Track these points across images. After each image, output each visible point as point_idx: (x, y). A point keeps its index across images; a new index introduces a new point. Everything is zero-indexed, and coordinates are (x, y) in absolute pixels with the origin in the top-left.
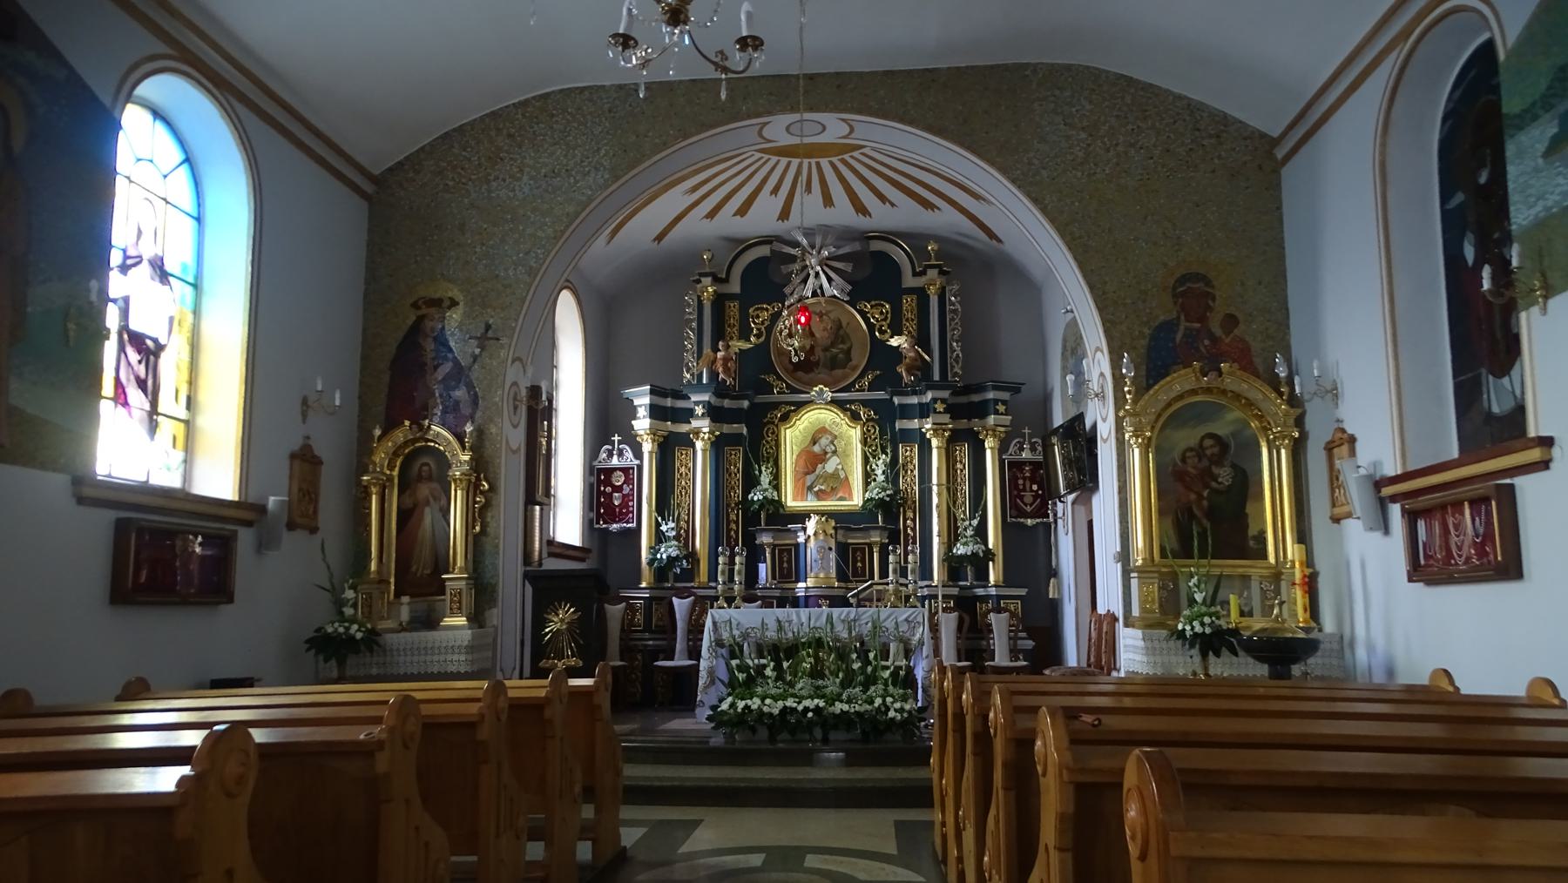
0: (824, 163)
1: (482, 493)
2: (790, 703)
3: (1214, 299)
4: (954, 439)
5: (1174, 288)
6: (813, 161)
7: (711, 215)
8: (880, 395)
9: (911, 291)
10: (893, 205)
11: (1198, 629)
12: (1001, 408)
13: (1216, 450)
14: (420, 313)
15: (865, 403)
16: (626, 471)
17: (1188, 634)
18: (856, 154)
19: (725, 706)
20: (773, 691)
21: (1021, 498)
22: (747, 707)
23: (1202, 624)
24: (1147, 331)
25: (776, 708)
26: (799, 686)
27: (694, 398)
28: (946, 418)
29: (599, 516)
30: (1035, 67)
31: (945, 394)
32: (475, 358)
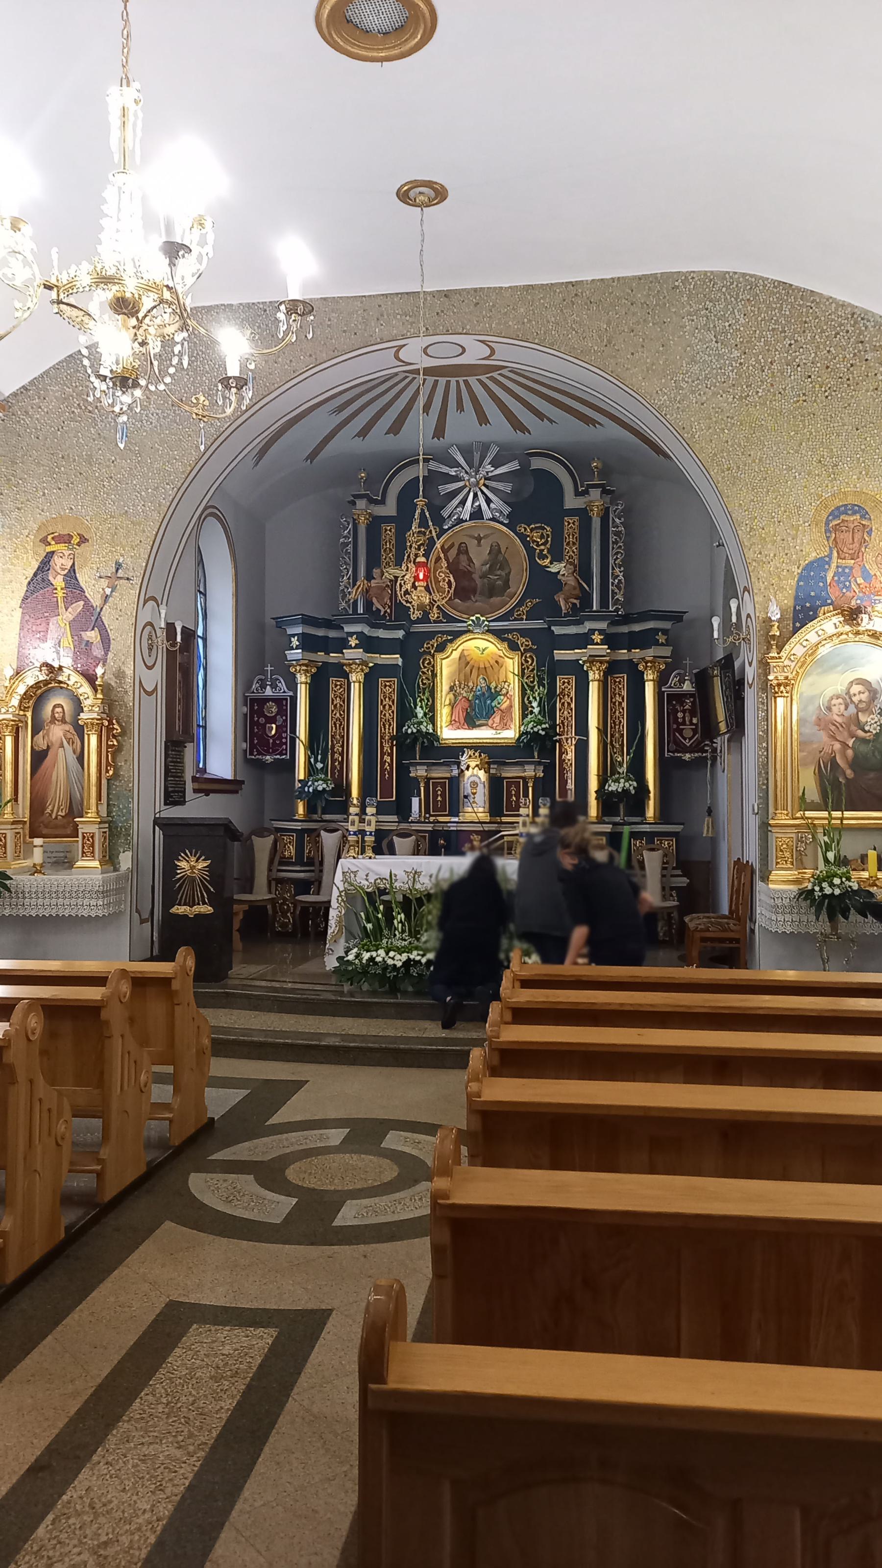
0: (472, 380)
1: (114, 736)
2: (414, 955)
3: (870, 533)
4: (612, 668)
5: (827, 524)
6: (461, 379)
7: (363, 433)
8: (538, 624)
9: (572, 512)
10: (551, 421)
11: (828, 891)
12: (662, 639)
13: (864, 697)
14: (49, 549)
15: (523, 633)
16: (279, 701)
17: (817, 894)
18: (495, 375)
19: (351, 957)
20: (400, 944)
21: (681, 732)
22: (372, 959)
23: (832, 885)
24: (797, 571)
25: (398, 960)
26: (424, 939)
27: (348, 628)
28: (603, 649)
29: (252, 746)
30: (686, 277)
31: (603, 625)
32: (106, 598)
